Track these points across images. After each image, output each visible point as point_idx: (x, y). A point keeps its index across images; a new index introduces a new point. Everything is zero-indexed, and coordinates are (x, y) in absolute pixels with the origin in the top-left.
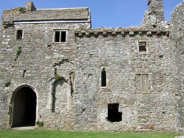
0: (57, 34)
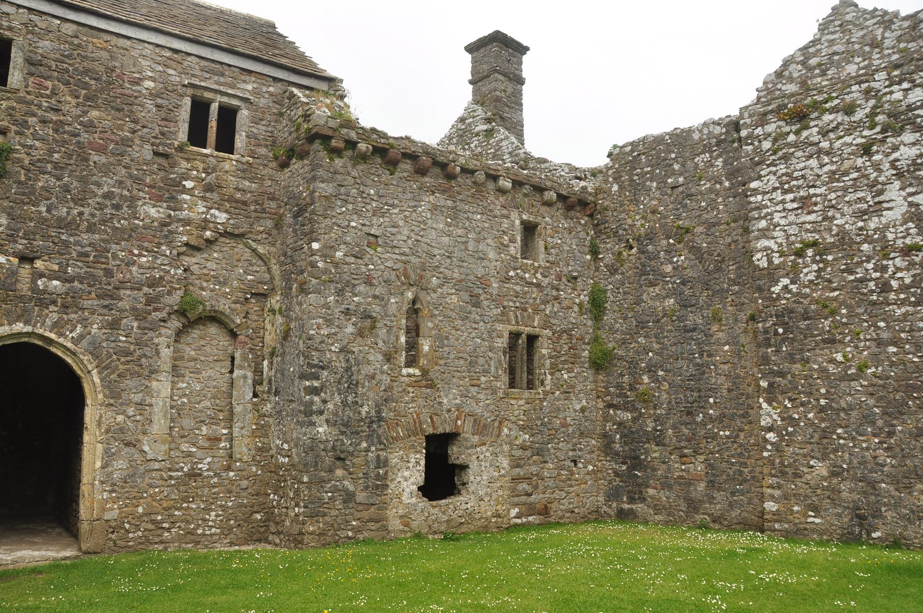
0: (200, 109)
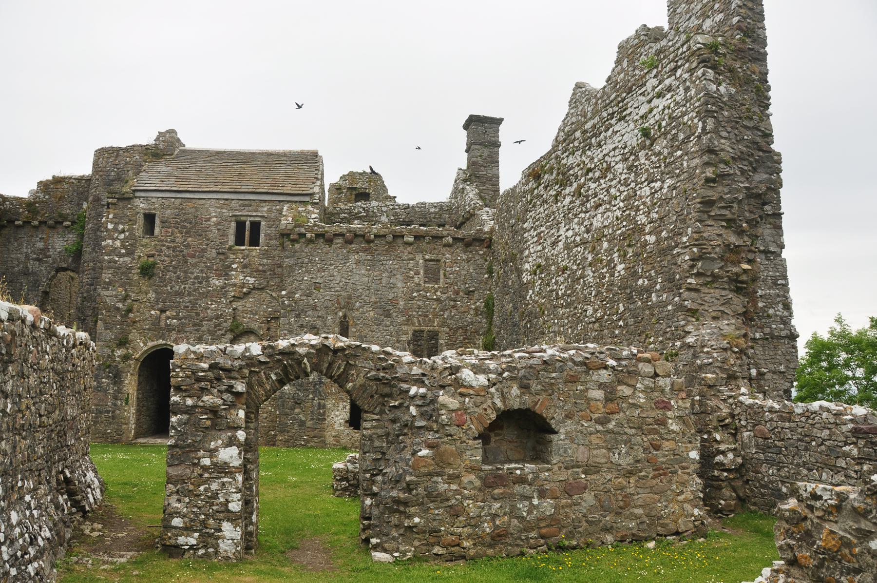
0: (240, 226)
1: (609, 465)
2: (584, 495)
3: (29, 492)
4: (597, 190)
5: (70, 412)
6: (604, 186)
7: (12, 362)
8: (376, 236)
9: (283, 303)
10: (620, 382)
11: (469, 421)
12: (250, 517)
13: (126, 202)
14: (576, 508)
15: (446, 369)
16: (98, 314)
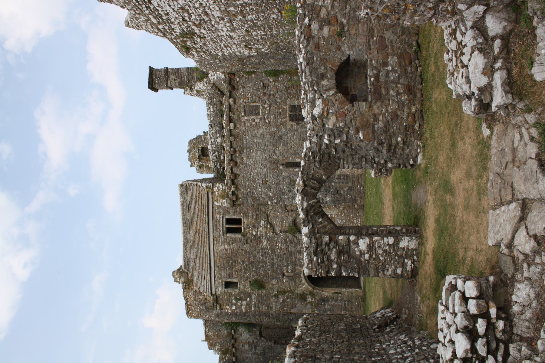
0: (229, 231)
1: (368, 22)
2: (386, 37)
3: (381, 345)
4: (196, 14)
5: (342, 327)
6: (193, 11)
7: (315, 356)
8: (231, 147)
9: (276, 203)
10: (318, 16)
11: (343, 110)
12: (398, 231)
13: (219, 299)
14: (394, 43)
15: (313, 123)
16: (287, 313)
